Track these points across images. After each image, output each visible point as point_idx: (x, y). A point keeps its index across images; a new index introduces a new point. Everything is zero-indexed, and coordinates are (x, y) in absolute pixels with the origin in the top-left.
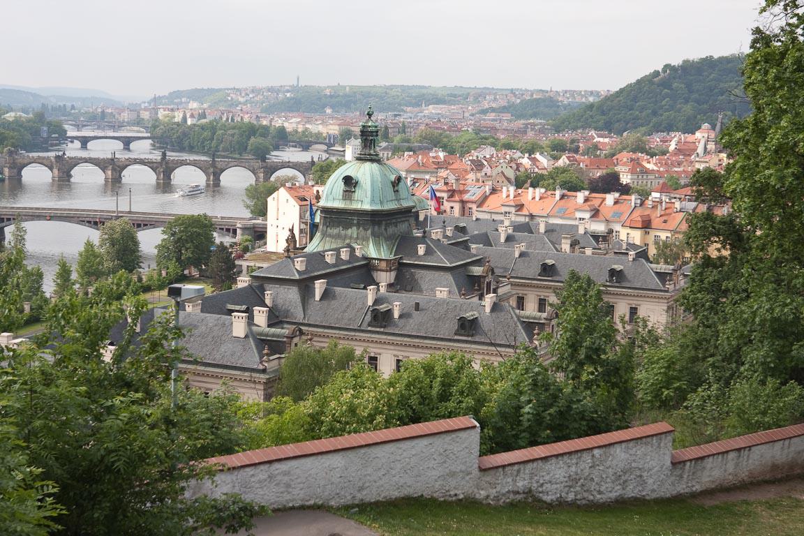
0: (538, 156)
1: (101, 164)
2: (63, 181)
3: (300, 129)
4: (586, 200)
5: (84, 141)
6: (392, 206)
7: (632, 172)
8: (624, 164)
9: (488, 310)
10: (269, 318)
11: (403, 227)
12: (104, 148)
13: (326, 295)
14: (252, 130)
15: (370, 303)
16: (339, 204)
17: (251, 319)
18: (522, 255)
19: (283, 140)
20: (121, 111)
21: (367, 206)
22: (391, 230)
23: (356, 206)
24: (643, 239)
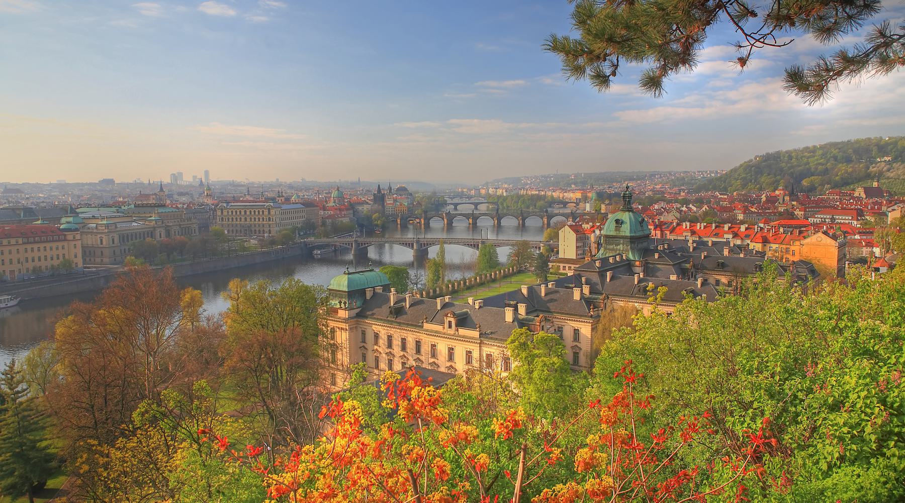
0: (691, 206)
1: (467, 216)
2: (450, 227)
3: (561, 196)
4: (730, 228)
5: (456, 205)
6: (639, 234)
7: (744, 213)
8: (739, 209)
9: (699, 286)
10: (527, 309)
11: (645, 244)
12: (466, 208)
13: (612, 279)
14: (535, 199)
15: (636, 283)
16: (613, 233)
17: (516, 309)
18: (705, 257)
19: (553, 202)
20: (470, 190)
21: (628, 234)
22: (640, 246)
23: (622, 234)
24: (763, 248)
